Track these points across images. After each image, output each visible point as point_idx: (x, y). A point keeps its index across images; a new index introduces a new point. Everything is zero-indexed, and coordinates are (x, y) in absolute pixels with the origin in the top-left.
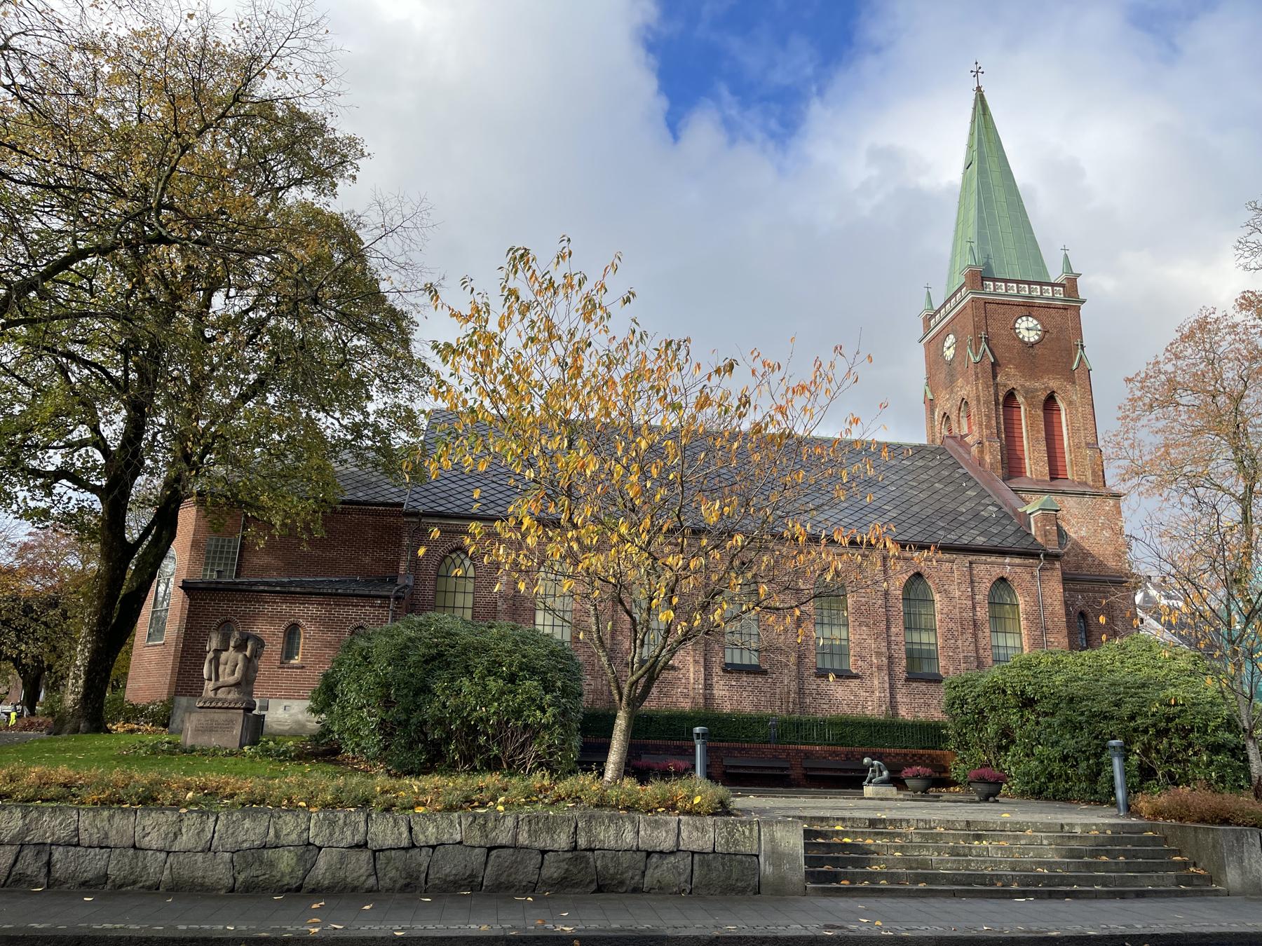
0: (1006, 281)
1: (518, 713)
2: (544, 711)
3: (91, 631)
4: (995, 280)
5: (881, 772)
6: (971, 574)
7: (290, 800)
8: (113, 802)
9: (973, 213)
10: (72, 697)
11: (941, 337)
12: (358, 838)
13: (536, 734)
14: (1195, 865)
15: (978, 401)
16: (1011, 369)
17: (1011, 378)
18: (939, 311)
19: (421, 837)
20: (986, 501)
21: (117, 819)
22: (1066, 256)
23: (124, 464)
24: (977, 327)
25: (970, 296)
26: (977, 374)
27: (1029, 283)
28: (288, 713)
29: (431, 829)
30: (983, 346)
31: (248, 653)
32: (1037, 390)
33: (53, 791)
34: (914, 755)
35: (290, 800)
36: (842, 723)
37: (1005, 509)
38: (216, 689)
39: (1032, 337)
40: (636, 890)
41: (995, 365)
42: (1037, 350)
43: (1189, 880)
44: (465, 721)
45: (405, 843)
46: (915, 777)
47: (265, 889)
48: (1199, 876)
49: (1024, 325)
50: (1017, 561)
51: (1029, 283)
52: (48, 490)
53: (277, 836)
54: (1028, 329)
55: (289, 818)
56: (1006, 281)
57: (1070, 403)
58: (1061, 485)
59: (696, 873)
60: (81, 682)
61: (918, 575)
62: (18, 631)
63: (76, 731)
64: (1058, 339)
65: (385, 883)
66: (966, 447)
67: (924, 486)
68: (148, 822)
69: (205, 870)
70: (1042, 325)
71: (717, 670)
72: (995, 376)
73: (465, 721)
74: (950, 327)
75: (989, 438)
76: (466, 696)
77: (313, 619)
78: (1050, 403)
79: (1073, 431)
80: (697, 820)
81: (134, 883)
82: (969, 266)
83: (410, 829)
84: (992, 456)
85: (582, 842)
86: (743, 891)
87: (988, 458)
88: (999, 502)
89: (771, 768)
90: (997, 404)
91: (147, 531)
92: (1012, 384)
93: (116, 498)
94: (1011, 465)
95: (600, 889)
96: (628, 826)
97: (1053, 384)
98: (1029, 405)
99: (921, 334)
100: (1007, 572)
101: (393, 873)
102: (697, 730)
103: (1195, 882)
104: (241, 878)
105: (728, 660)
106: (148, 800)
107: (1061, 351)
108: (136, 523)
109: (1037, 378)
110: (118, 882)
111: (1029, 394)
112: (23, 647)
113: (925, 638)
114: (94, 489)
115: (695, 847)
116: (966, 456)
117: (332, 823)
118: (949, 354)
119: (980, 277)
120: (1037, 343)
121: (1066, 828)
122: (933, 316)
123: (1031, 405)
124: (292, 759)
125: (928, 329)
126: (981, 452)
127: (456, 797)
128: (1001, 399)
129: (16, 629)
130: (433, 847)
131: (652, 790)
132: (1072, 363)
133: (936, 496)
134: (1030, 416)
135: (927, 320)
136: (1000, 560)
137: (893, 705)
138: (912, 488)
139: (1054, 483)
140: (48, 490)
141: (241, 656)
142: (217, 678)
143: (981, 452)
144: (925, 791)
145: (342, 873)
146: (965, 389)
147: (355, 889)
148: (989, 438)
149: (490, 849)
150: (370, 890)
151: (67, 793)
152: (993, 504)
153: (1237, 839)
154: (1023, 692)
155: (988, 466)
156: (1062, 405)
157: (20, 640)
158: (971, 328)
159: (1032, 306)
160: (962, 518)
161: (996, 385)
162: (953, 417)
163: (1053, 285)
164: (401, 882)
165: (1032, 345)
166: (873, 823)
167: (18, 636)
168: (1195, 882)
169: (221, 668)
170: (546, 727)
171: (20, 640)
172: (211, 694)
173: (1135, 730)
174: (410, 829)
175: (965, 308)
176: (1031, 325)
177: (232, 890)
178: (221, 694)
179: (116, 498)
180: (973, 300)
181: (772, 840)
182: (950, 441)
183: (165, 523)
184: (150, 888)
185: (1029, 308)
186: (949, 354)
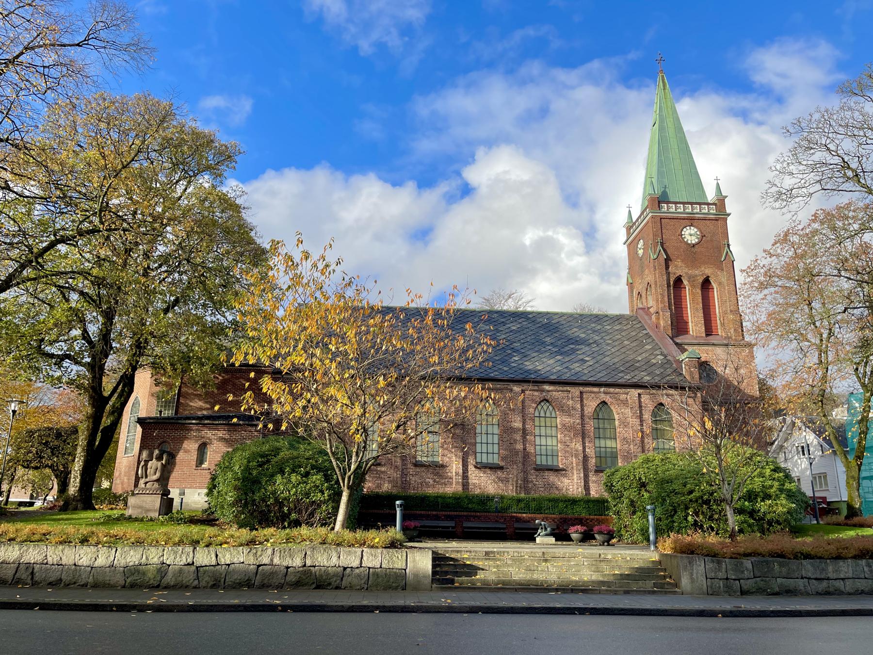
0: (676, 203)
1: (307, 495)
2: (322, 492)
4: (668, 202)
5: (546, 529)
6: (640, 402)
7: (157, 542)
8: (66, 542)
9: (656, 157)
10: (73, 489)
11: (636, 241)
12: (190, 560)
13: (319, 506)
14: (670, 577)
15: (656, 284)
16: (679, 263)
17: (678, 268)
18: (635, 223)
19: (223, 560)
20: (658, 352)
21: (66, 550)
22: (718, 184)
23: (101, 348)
24: (655, 235)
25: (651, 214)
26: (655, 267)
27: (692, 204)
28: (194, 497)
29: (228, 556)
30: (659, 247)
31: (164, 462)
32: (696, 276)
33: (37, 537)
35: (157, 542)
36: (566, 501)
37: (669, 358)
38: (146, 483)
39: (694, 240)
40: (337, 588)
41: (668, 260)
42: (696, 249)
43: (662, 586)
44: (276, 499)
45: (214, 563)
46: (576, 532)
47: (141, 586)
48: (669, 583)
51: (692, 204)
52: (59, 364)
53: (147, 559)
54: (690, 235)
55: (153, 549)
56: (676, 203)
57: (720, 284)
58: (712, 340)
59: (371, 579)
60: (78, 480)
62: (52, 449)
64: (712, 241)
65: (203, 584)
66: (649, 315)
67: (618, 342)
68: (82, 552)
69: (111, 576)
70: (701, 231)
71: (471, 468)
72: (667, 267)
73: (276, 499)
76: (285, 486)
77: (221, 439)
78: (706, 284)
79: (722, 303)
80: (373, 551)
81: (75, 583)
82: (650, 194)
83: (217, 556)
84: (665, 321)
85: (308, 563)
86: (396, 588)
87: (662, 323)
88: (666, 352)
89: (495, 528)
90: (669, 286)
91: (115, 390)
92: (679, 273)
93: (97, 369)
94: (679, 326)
95: (318, 587)
96: (334, 554)
97: (708, 271)
99: (625, 239)
101: (207, 579)
102: (398, 502)
103: (666, 586)
104: (128, 581)
105: (479, 460)
106: (84, 541)
107: (715, 247)
108: (108, 384)
110: (67, 583)
111: (692, 279)
112: (55, 459)
113: (610, 443)
114: (83, 365)
115: (370, 565)
116: (649, 322)
117: (176, 553)
118: (641, 252)
120: (697, 244)
121: (602, 556)
122: (631, 227)
123: (693, 286)
124: (185, 523)
125: (629, 234)
126: (658, 319)
127: (243, 540)
128: (672, 283)
129: (50, 448)
130: (229, 565)
131: (359, 534)
133: (623, 350)
134: (692, 294)
135: (629, 229)
137: (587, 488)
138: (608, 344)
139: (710, 337)
140: (59, 364)
141: (159, 464)
142: (146, 477)
143: (658, 319)
144: (608, 542)
145: (180, 578)
146: (649, 277)
147: (187, 587)
149: (259, 566)
150: (195, 587)
151: (44, 538)
152: (661, 354)
153: (690, 563)
154: (640, 479)
155: (662, 328)
156: (714, 285)
157: (53, 454)
158: (651, 236)
160: (637, 365)
161: (668, 274)
162: (644, 295)
163: (708, 204)
164: (212, 583)
165: (694, 246)
166: (487, 553)
167: (52, 452)
168: (666, 586)
169: (149, 471)
170: (325, 502)
171: (53, 454)
172: (143, 486)
173: (691, 501)
174: (217, 556)
175: (648, 222)
176: (692, 232)
177: (124, 587)
179: (97, 369)
180: (652, 217)
181: (414, 561)
182: (641, 311)
183: (127, 383)
184: (83, 586)
185: (691, 220)
186: (641, 252)
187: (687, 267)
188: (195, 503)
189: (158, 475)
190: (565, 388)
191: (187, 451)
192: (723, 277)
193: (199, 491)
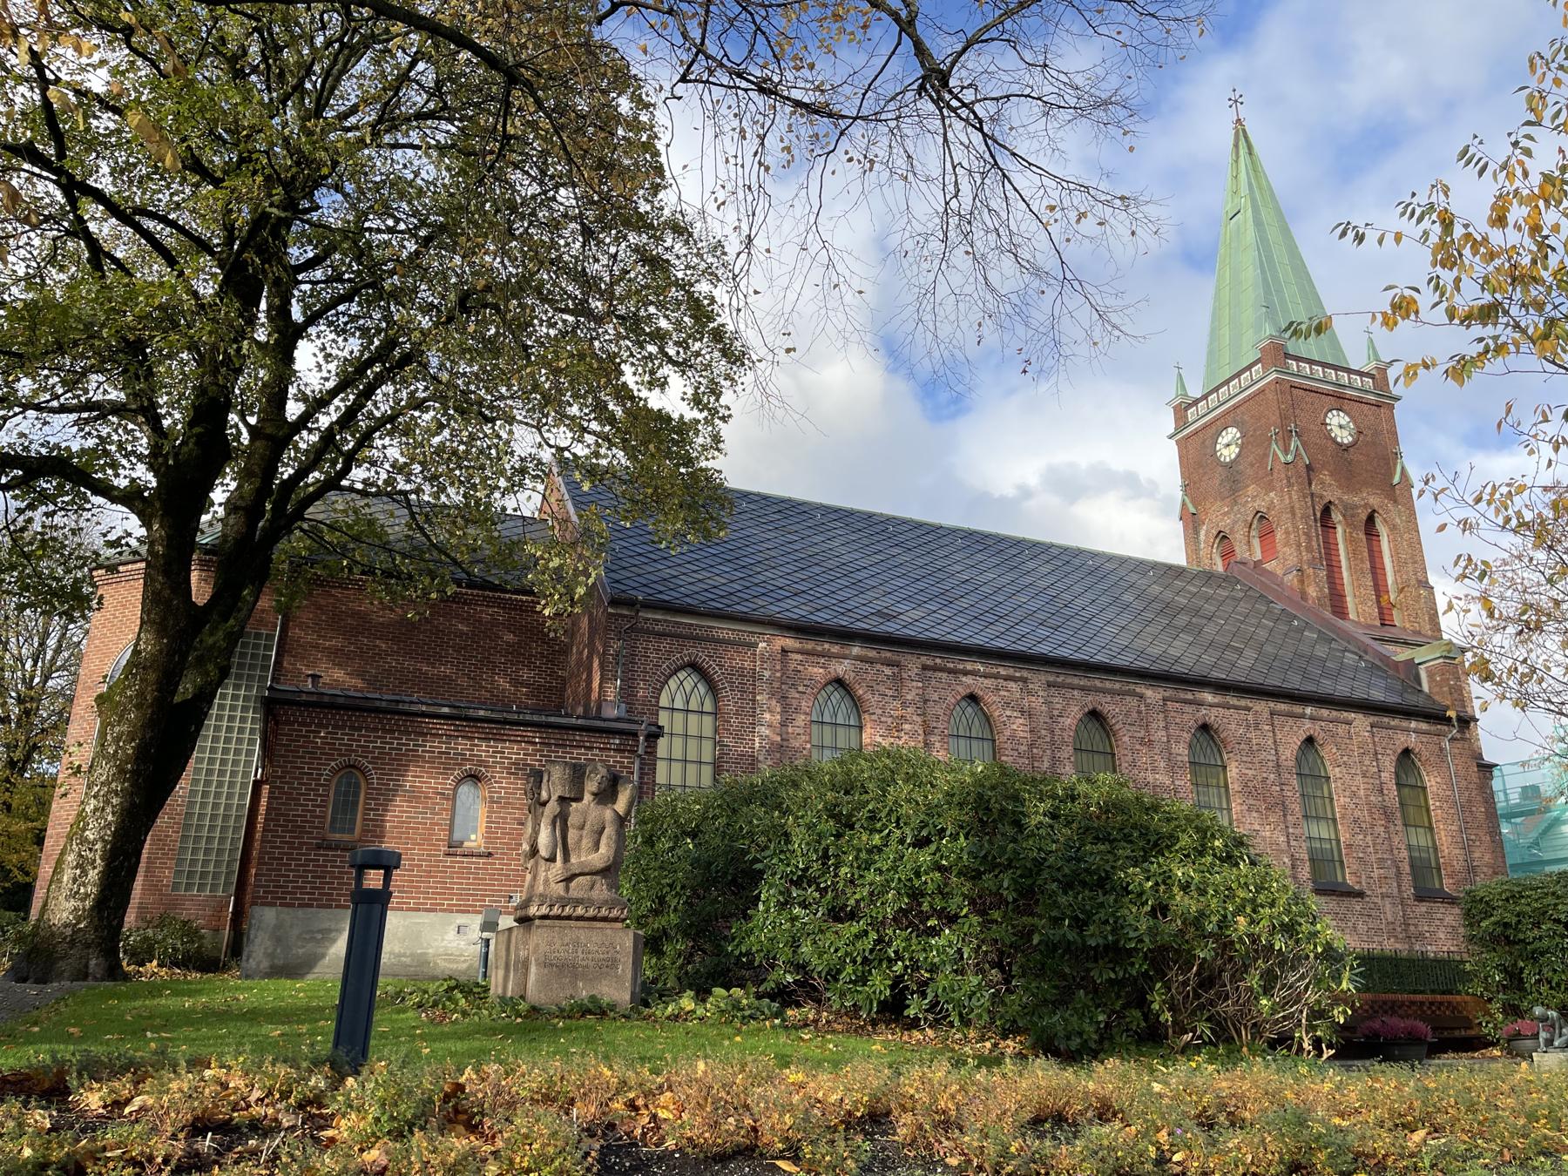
3: (121, 771)
17: (1330, 491)
25: (1274, 376)
32: (1357, 507)
34: (1432, 1003)
38: (568, 880)
39: (1345, 437)
41: (1309, 468)
42: (1353, 455)
49: (1335, 421)
50: (1424, 726)
54: (1340, 426)
57: (1393, 528)
60: (93, 875)
61: (1310, 740)
63: (82, 975)
74: (1229, 418)
75: (1311, 563)
87: (1312, 592)
97: (1374, 501)
98: (1348, 525)
99: (1172, 431)
100: (1412, 740)
109: (1357, 491)
119: (1276, 354)
132: (1392, 476)
134: (1350, 540)
136: (1405, 724)
142: (566, 859)
148: (1311, 563)
158: (1275, 418)
159: (1340, 397)
165: (1346, 448)
169: (572, 835)
175: (1261, 391)
176: (1343, 422)
178: (579, 887)
180: (1277, 381)
185: (1339, 399)
187: (1340, 486)
188: (449, 956)
189: (605, 851)
190: (1243, 703)
191: (415, 797)
192: (1396, 515)
193: (461, 919)
